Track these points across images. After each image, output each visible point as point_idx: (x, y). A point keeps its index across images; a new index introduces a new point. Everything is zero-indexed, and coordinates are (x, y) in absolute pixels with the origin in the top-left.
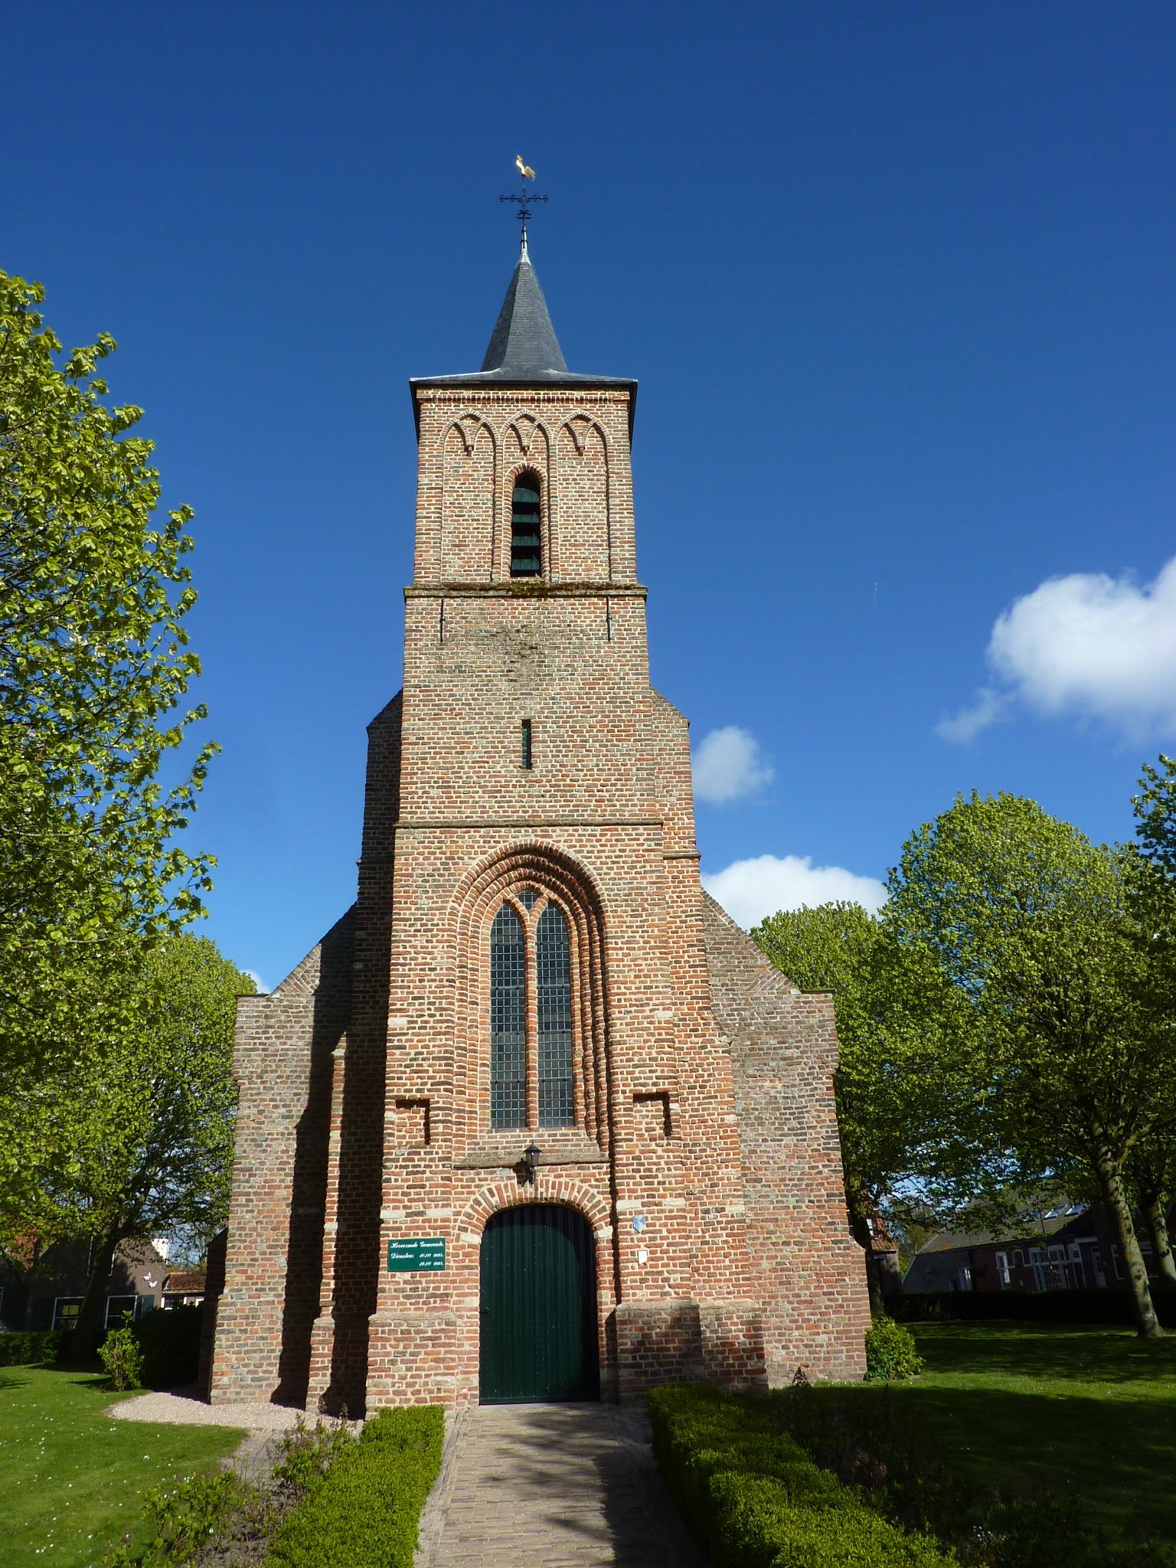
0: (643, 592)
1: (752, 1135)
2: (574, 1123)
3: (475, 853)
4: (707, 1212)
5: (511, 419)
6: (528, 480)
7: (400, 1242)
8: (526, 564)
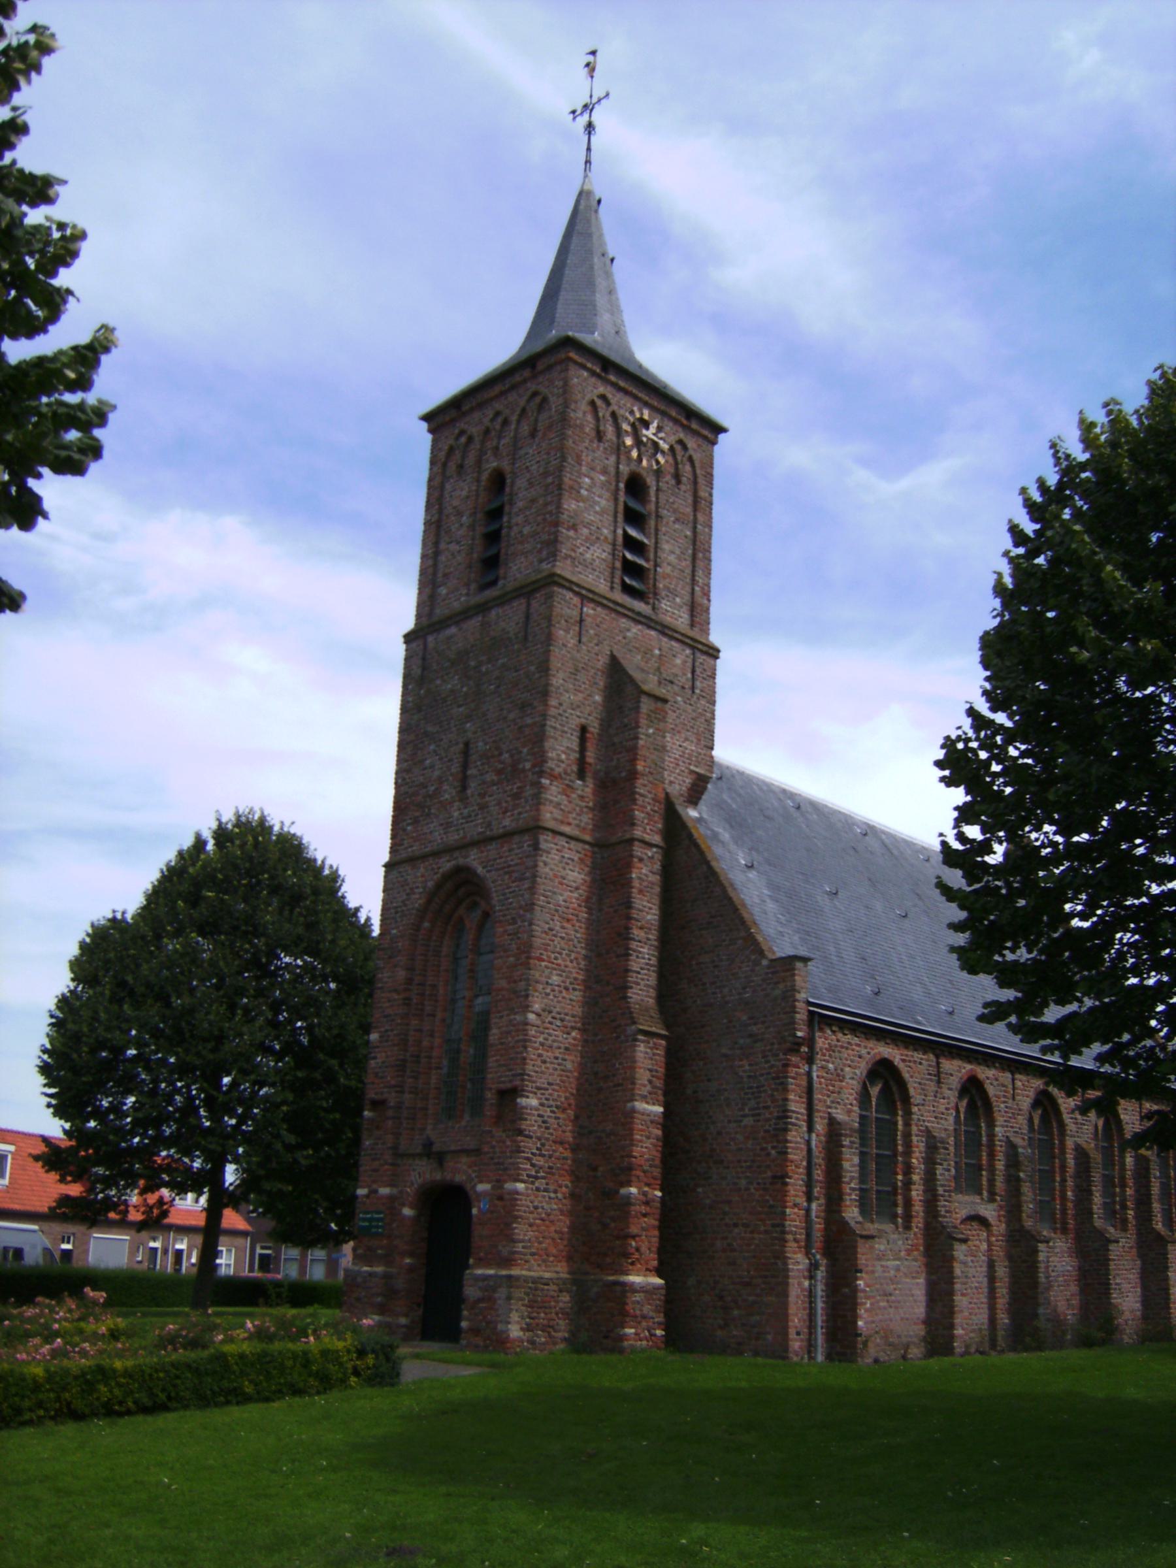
6: (499, 481)
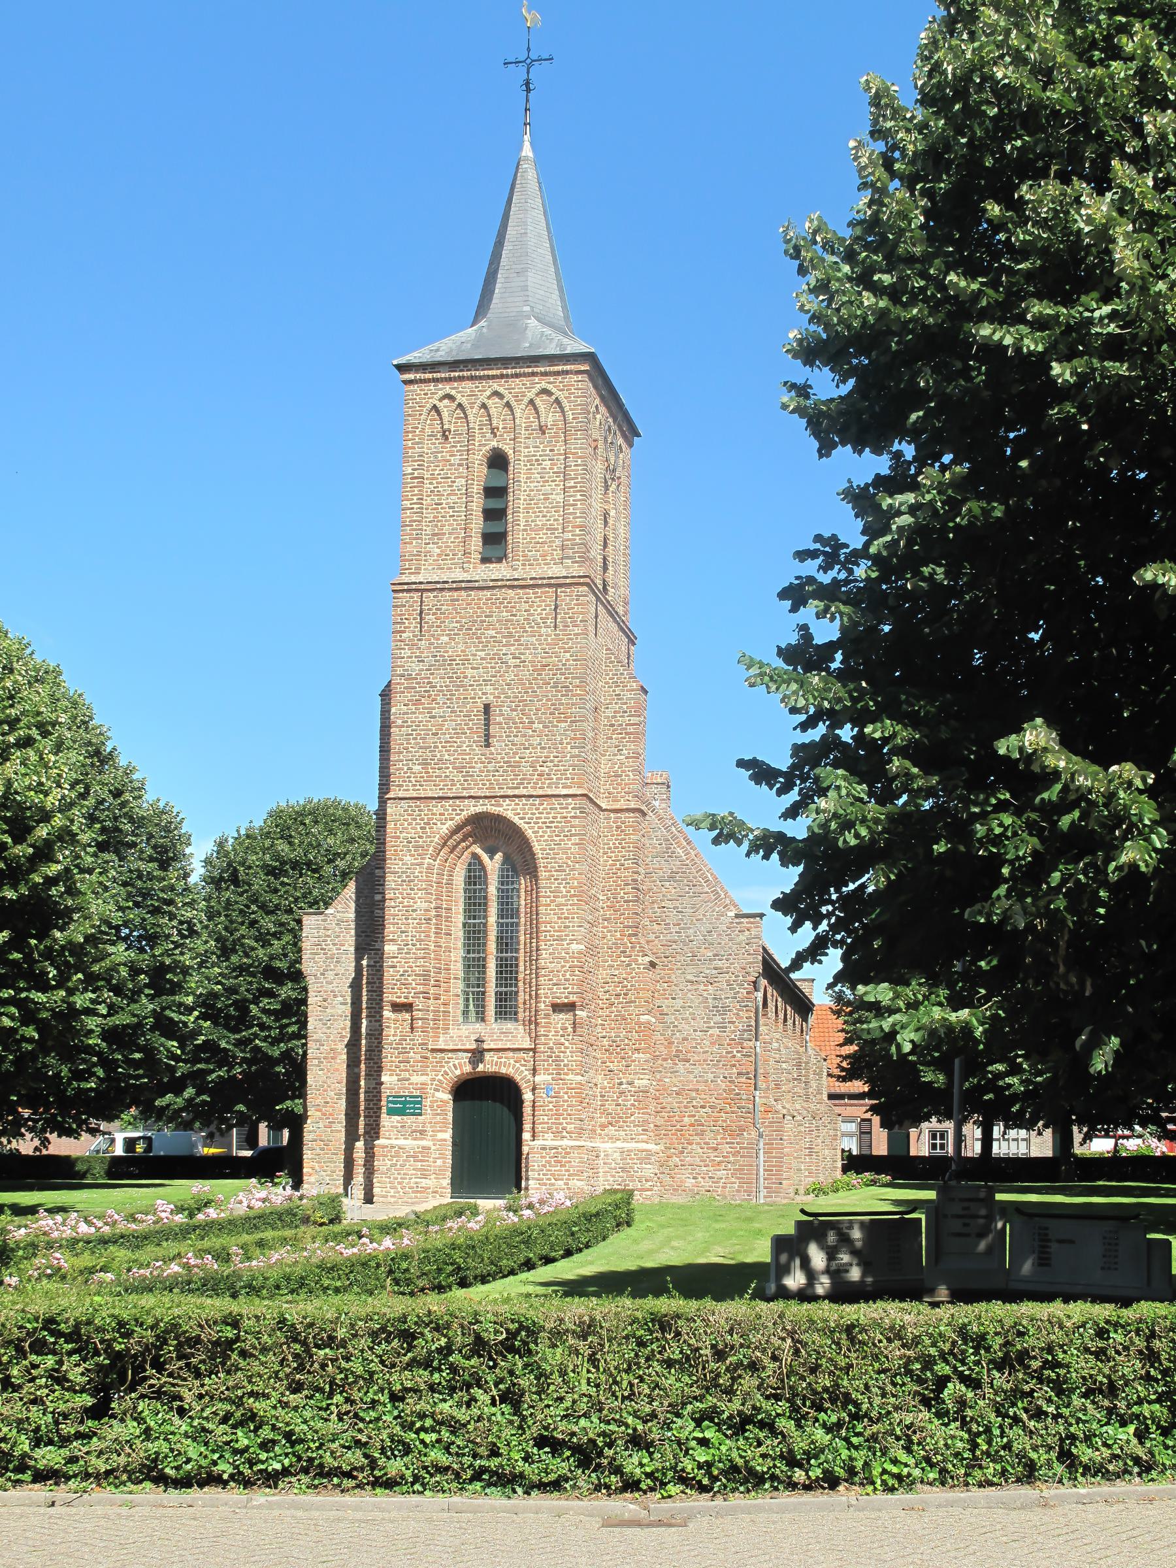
0: (588, 580)
1: (687, 1027)
2: (516, 1020)
3: (446, 820)
4: (621, 1084)
5: (483, 398)
6: (498, 461)
7: (394, 1097)
8: (494, 551)
